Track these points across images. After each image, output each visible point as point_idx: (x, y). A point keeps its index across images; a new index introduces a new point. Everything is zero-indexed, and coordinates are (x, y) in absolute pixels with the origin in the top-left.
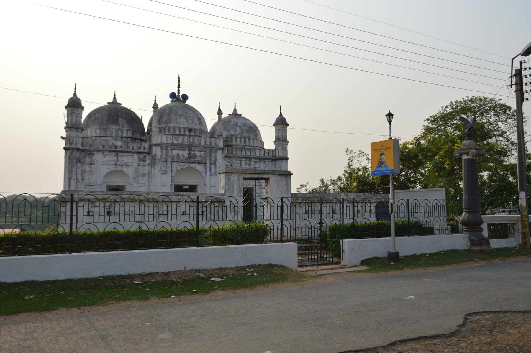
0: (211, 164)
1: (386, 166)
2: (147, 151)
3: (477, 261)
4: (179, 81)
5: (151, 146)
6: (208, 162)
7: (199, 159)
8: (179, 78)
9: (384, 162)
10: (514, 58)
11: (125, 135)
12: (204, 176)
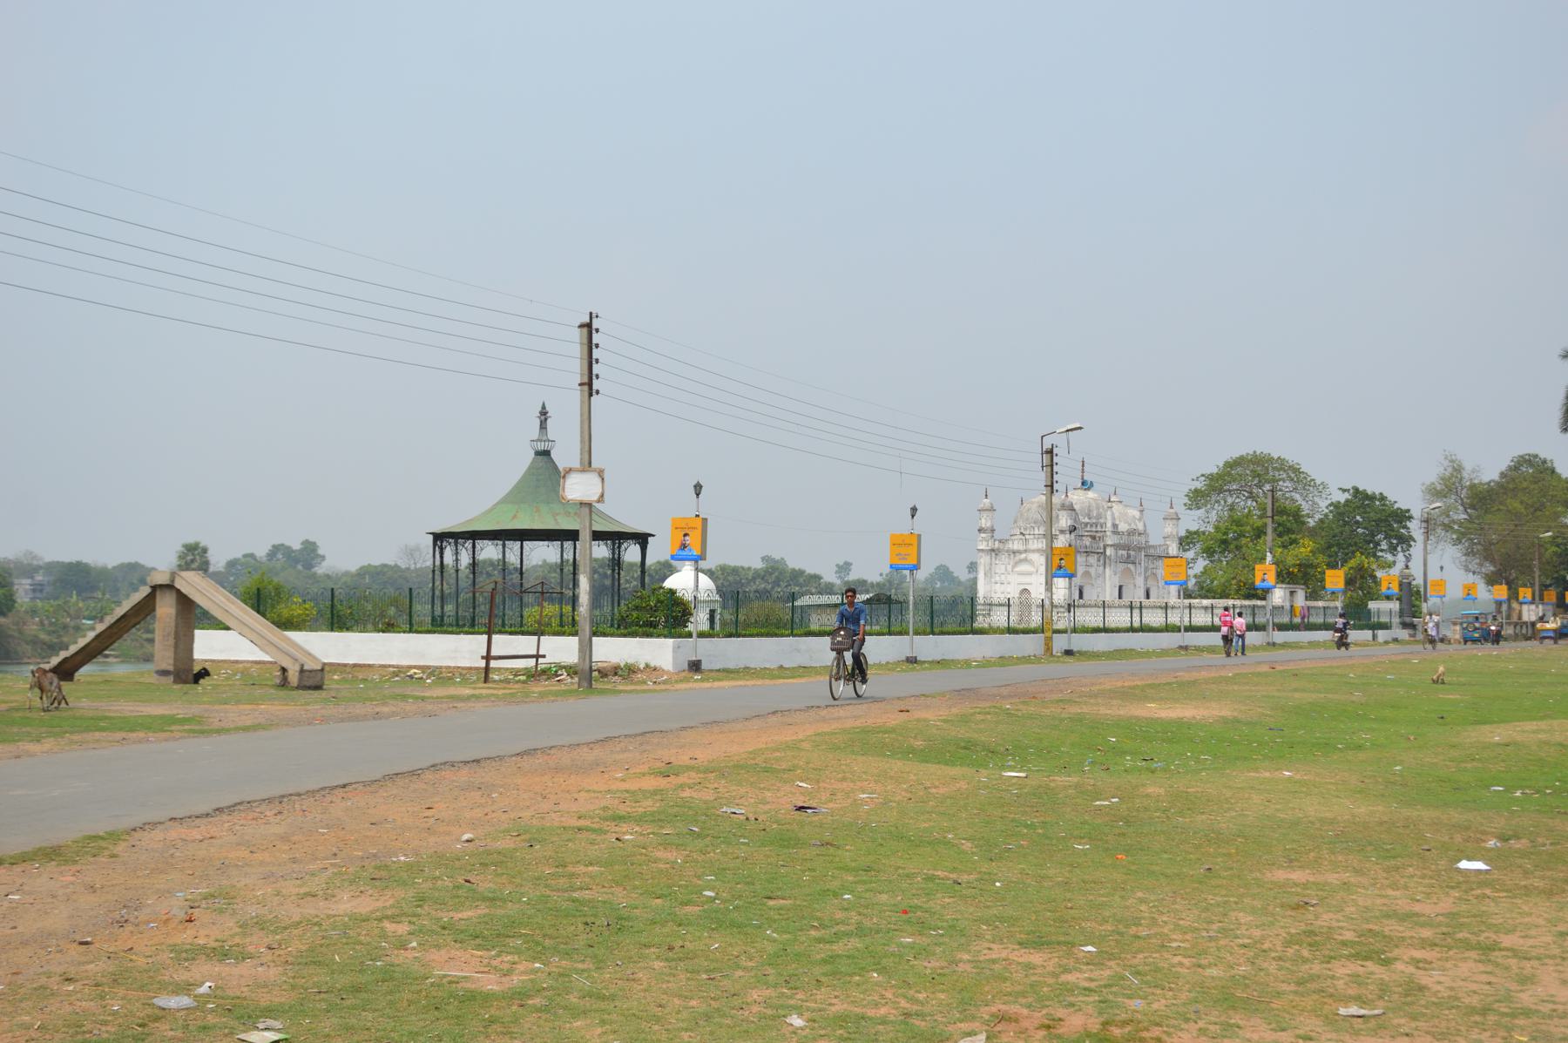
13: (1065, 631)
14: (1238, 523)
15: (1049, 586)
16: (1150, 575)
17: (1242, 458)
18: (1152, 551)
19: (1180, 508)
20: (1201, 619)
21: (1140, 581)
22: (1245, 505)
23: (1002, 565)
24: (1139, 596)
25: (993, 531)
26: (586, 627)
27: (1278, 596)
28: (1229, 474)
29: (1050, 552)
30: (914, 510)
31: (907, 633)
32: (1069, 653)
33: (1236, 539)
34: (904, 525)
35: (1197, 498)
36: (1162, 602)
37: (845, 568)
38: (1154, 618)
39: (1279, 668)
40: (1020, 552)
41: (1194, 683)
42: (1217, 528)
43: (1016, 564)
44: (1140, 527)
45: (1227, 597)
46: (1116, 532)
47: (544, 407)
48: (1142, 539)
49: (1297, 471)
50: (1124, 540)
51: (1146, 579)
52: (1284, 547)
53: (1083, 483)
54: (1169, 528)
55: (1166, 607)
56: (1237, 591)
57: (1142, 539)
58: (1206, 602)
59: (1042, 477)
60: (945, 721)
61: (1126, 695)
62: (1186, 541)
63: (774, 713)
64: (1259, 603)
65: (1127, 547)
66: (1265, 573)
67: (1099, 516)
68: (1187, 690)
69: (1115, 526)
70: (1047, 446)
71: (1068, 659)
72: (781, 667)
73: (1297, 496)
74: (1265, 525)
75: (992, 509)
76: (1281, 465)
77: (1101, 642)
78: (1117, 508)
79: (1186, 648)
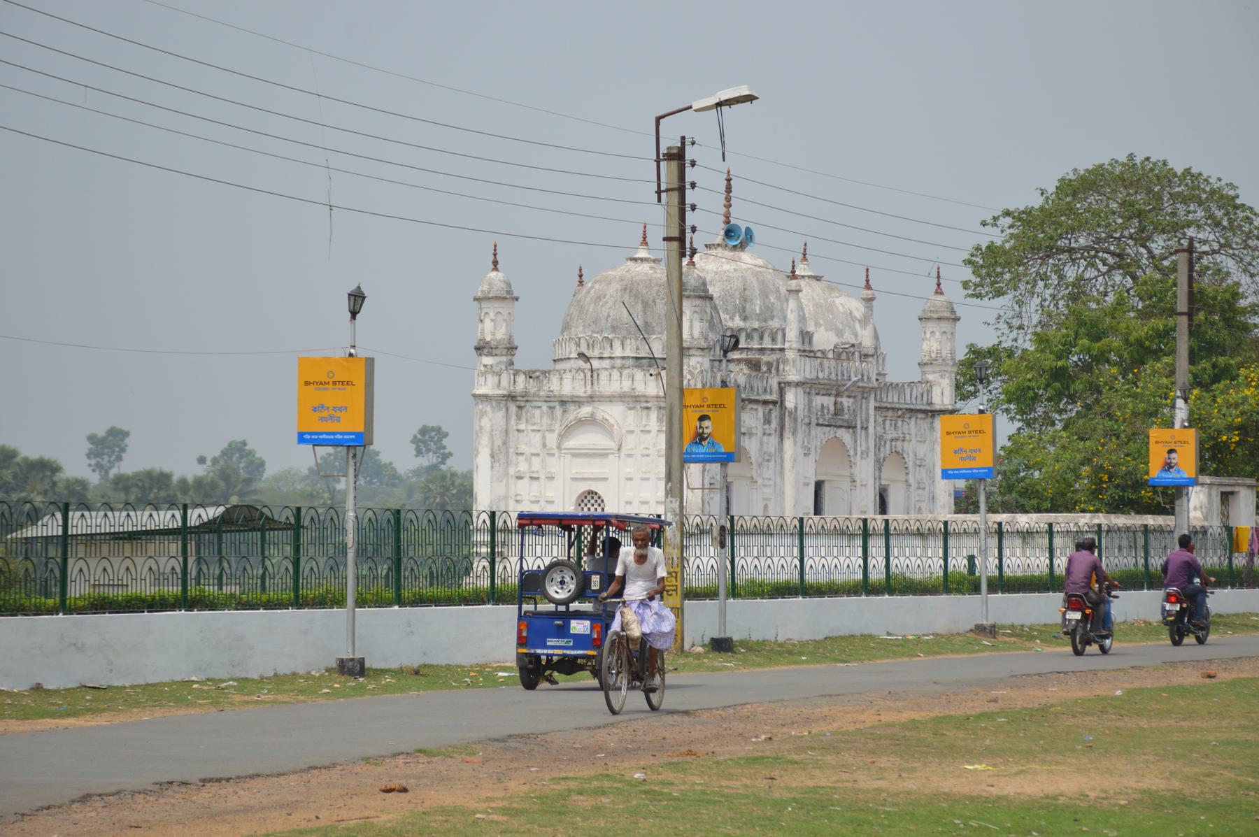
2: (774, 397)
4: (729, 189)
7: (846, 417)
10: (663, 117)
11: (618, 352)
13: (711, 594)
15: (674, 483)
16: (890, 456)
17: (1099, 171)
18: (892, 398)
19: (954, 292)
20: (1025, 560)
21: (865, 470)
22: (1107, 287)
23: (534, 433)
24: (865, 505)
25: (512, 349)
26: (350, 600)
27: (1198, 506)
28: (1071, 210)
29: (676, 405)
30: (357, 299)
31: (338, 602)
32: (721, 645)
33: (1088, 368)
34: (331, 336)
35: (992, 269)
37: (110, 443)
38: (914, 560)
39: (1223, 676)
40: (577, 401)
41: (1044, 711)
42: (1041, 340)
43: (568, 430)
44: (866, 339)
45: (1069, 508)
46: (807, 352)
48: (871, 368)
49: (1230, 203)
50: (828, 371)
51: (879, 464)
52: (1206, 387)
53: (729, 233)
54: (933, 342)
55: (946, 534)
56: (1095, 493)
58: (1024, 520)
59: (658, 218)
60: (504, 811)
61: (906, 742)
62: (975, 370)
63: (85, 799)
64: (1151, 520)
65: (834, 389)
66: (1172, 448)
68: (1031, 731)
69: (805, 336)
70: (670, 141)
71: (720, 660)
72: (38, 688)
73: (1229, 264)
74: (1166, 335)
75: (508, 297)
76: (1193, 188)
77: (793, 620)
78: (810, 292)
79: (989, 631)
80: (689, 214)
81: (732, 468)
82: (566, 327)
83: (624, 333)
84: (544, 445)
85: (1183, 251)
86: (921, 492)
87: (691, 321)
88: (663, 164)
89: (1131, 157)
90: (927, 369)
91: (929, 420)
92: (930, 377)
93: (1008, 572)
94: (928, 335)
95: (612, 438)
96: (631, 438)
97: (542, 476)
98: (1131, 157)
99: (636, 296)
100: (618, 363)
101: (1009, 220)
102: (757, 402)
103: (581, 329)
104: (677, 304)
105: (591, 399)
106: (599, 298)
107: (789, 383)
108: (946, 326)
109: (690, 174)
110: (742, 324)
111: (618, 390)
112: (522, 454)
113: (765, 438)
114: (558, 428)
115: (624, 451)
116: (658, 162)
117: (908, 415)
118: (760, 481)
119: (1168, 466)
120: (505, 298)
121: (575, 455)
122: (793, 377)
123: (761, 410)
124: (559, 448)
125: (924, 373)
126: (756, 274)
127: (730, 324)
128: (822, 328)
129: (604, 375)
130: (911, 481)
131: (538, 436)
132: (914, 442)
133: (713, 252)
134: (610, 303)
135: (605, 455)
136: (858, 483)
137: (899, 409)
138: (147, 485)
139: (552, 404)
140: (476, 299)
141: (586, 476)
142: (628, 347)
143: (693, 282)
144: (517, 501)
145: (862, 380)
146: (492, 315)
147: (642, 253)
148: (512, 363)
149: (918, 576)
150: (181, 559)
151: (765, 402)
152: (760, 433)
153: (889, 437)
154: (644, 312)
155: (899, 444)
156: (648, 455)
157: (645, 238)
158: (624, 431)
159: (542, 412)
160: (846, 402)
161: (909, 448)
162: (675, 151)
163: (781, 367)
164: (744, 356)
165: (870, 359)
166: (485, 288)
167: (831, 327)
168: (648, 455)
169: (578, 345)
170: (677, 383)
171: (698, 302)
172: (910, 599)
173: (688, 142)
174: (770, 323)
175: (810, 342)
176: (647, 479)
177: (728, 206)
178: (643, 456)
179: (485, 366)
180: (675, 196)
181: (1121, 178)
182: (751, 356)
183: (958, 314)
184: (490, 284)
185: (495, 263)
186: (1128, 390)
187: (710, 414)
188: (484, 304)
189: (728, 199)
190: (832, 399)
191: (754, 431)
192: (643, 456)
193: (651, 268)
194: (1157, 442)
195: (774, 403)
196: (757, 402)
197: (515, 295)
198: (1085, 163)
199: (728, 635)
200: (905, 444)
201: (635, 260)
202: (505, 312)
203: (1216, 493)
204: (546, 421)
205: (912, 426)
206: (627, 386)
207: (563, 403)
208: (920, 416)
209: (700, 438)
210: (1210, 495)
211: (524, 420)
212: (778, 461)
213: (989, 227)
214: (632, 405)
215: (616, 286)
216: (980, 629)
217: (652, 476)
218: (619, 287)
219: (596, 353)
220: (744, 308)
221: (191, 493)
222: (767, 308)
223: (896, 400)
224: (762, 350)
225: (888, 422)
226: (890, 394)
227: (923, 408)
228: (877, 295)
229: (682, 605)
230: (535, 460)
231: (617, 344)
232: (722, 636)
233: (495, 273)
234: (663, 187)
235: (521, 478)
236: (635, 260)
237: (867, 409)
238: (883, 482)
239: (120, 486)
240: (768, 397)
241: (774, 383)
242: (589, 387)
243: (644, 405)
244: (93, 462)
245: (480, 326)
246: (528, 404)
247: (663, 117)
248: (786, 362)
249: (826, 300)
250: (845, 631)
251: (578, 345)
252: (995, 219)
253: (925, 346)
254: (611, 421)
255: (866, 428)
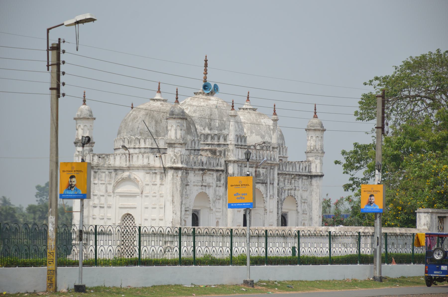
0: (270, 184)
1: (77, 190)
2: (222, 168)
3: (276, 281)
4: (206, 65)
5: (227, 163)
6: (269, 183)
7: (262, 178)
8: (206, 61)
9: (75, 185)
10: (51, 29)
11: (143, 145)
12: (265, 199)
14: (414, 137)
18: (289, 169)
36: (261, 229)
40: (122, 169)
43: (118, 184)
44: (274, 140)
47: (95, 20)
48: (276, 155)
51: (280, 202)
53: (205, 87)
55: (266, 237)
57: (276, 155)
59: (47, 78)
67: (223, 126)
69: (241, 138)
70: (53, 41)
75: (90, 118)
79: (250, 284)
80: (62, 77)
81: (85, 201)
82: (119, 133)
83: (146, 136)
84: (107, 191)
85: (379, 96)
86: (304, 215)
87: (176, 130)
88: (50, 52)
89: (438, 51)
90: (309, 155)
91: (310, 180)
92: (311, 159)
93: (270, 255)
94: (309, 138)
95: (138, 188)
96: (147, 188)
97: (105, 206)
98: (438, 51)
99: (152, 118)
100: (143, 150)
101: (378, 82)
102: (213, 170)
103: (125, 133)
104: (55, 121)
105: (129, 168)
106: (134, 118)
107: (230, 161)
108: (318, 133)
109: (63, 57)
110: (209, 132)
111: (142, 164)
112: (96, 195)
113: (218, 188)
114: (113, 182)
115: (144, 194)
116: (48, 50)
117: (297, 177)
118: (214, 209)
119: (370, 203)
120: (88, 119)
121: (121, 196)
122: (232, 158)
123: (215, 174)
124: (113, 192)
125: (308, 157)
126: (211, 108)
127: (203, 132)
128: (254, 134)
129: (135, 157)
130: (299, 210)
131: (104, 186)
132: (301, 190)
133: (198, 96)
134: (140, 121)
135: (135, 196)
136: (268, 211)
137: (292, 174)
138: (44, 210)
139: (110, 171)
140: (75, 119)
141: (126, 206)
142: (147, 143)
143: (177, 111)
144: (94, 218)
145: (271, 160)
146: (82, 127)
147: (158, 96)
148: (92, 150)
149: (217, 257)
150: (94, 246)
151: (217, 171)
152: (214, 185)
153: (287, 188)
154: (156, 126)
155: (293, 192)
156: (155, 196)
157: (159, 89)
158: (144, 185)
159: (106, 175)
160: (262, 171)
161: (298, 194)
162: (55, 46)
163: (226, 153)
164: (210, 148)
165: (275, 150)
166: (79, 113)
167: (258, 134)
168: (155, 196)
169: (124, 142)
170: (54, 159)
171: (179, 121)
172: (311, 267)
173: (61, 41)
174: (223, 131)
175: (245, 141)
176: (155, 208)
177: (206, 73)
178: (153, 196)
179: (78, 152)
180: (55, 67)
181: (433, 61)
182: (213, 148)
183: (325, 128)
184: (81, 112)
185: (84, 101)
186: (417, 165)
187: (75, 175)
188: (79, 121)
189: (206, 70)
190: (254, 169)
191: (211, 185)
192: (153, 196)
193: (161, 104)
194: (365, 191)
195: (222, 171)
196: (213, 170)
197: (94, 117)
198: (417, 54)
199: (83, 284)
200: (296, 192)
201: (154, 100)
202: (88, 125)
203: (435, 217)
204: (107, 179)
205: (300, 183)
206: (145, 162)
207: (116, 170)
208: (304, 178)
209: (70, 187)
210: (432, 218)
211: (97, 178)
212: (224, 199)
213: (368, 85)
214: (148, 171)
215: (143, 112)
216: (246, 283)
217: (157, 207)
218: (144, 113)
219: (132, 146)
220: (210, 124)
221: (66, 214)
222: (222, 124)
223: (291, 170)
224: (219, 145)
225: (286, 181)
226: (288, 167)
227: (306, 174)
228: (279, 118)
229: (56, 269)
230: (102, 198)
231: (142, 141)
232: (80, 284)
233: (84, 106)
234: (50, 63)
235: (95, 207)
236: (154, 100)
237: (273, 174)
238: (283, 211)
239: (31, 211)
240: (219, 168)
241: (222, 161)
242: (128, 162)
243: (154, 171)
244: (39, 199)
245: (77, 132)
246: (99, 171)
247: (51, 29)
248: (229, 151)
249: (257, 120)
250: (166, 283)
251: (124, 142)
252: (371, 81)
253: (308, 144)
254: (138, 179)
255: (273, 184)
